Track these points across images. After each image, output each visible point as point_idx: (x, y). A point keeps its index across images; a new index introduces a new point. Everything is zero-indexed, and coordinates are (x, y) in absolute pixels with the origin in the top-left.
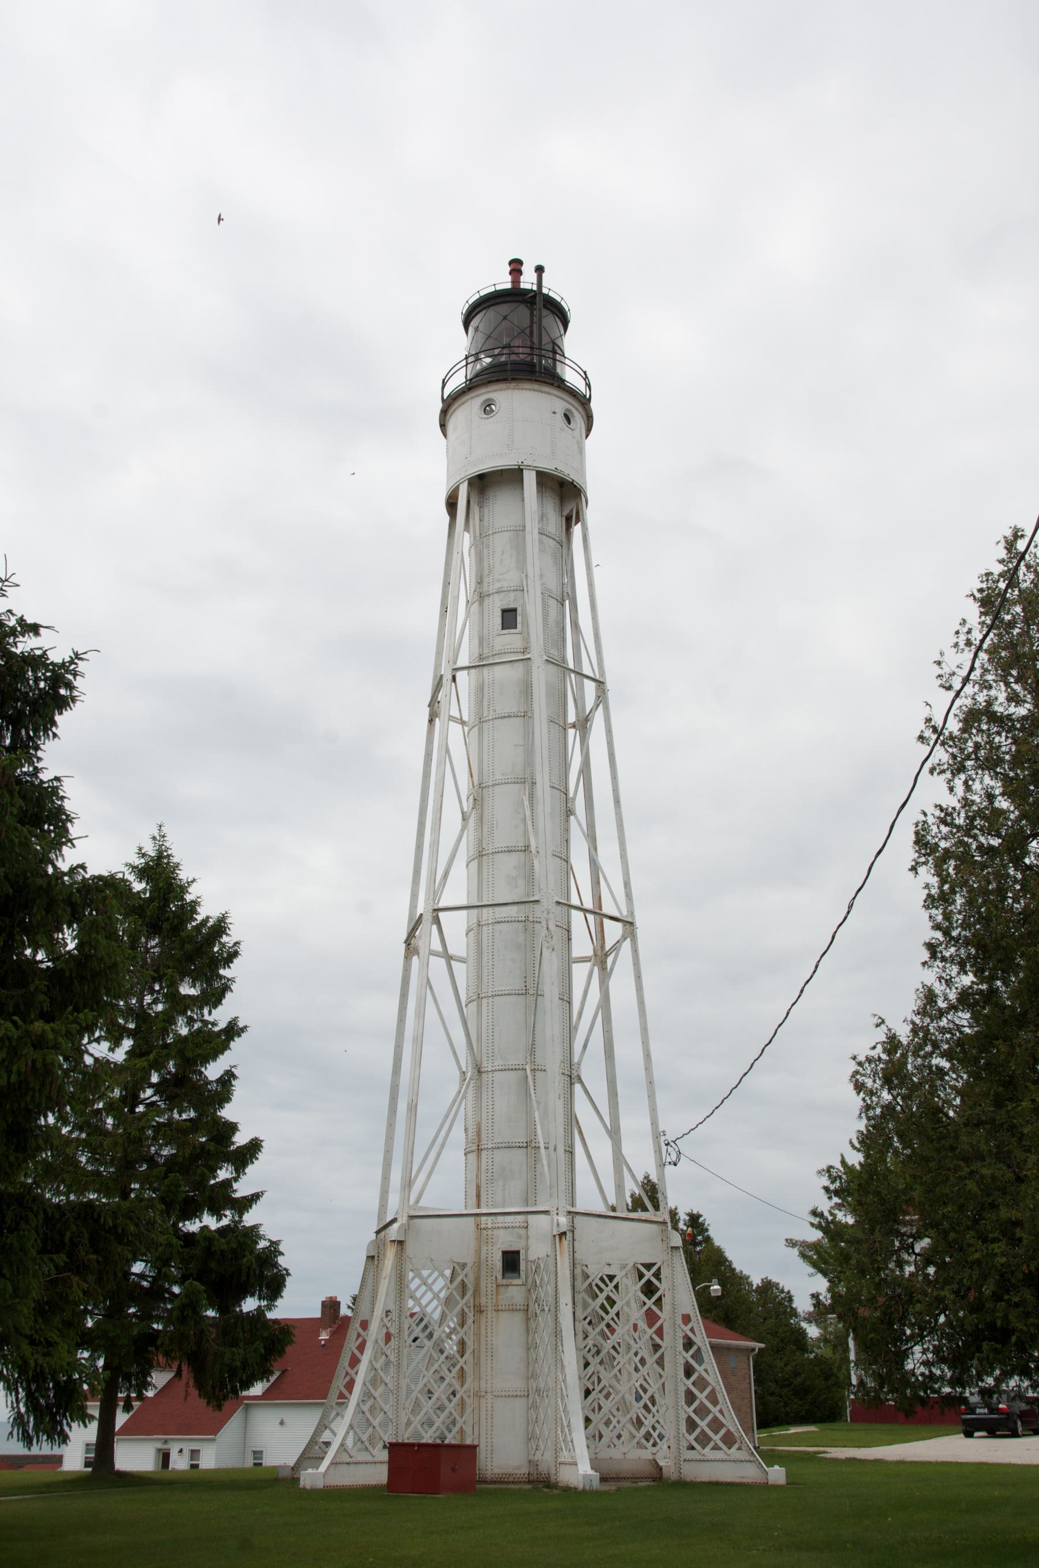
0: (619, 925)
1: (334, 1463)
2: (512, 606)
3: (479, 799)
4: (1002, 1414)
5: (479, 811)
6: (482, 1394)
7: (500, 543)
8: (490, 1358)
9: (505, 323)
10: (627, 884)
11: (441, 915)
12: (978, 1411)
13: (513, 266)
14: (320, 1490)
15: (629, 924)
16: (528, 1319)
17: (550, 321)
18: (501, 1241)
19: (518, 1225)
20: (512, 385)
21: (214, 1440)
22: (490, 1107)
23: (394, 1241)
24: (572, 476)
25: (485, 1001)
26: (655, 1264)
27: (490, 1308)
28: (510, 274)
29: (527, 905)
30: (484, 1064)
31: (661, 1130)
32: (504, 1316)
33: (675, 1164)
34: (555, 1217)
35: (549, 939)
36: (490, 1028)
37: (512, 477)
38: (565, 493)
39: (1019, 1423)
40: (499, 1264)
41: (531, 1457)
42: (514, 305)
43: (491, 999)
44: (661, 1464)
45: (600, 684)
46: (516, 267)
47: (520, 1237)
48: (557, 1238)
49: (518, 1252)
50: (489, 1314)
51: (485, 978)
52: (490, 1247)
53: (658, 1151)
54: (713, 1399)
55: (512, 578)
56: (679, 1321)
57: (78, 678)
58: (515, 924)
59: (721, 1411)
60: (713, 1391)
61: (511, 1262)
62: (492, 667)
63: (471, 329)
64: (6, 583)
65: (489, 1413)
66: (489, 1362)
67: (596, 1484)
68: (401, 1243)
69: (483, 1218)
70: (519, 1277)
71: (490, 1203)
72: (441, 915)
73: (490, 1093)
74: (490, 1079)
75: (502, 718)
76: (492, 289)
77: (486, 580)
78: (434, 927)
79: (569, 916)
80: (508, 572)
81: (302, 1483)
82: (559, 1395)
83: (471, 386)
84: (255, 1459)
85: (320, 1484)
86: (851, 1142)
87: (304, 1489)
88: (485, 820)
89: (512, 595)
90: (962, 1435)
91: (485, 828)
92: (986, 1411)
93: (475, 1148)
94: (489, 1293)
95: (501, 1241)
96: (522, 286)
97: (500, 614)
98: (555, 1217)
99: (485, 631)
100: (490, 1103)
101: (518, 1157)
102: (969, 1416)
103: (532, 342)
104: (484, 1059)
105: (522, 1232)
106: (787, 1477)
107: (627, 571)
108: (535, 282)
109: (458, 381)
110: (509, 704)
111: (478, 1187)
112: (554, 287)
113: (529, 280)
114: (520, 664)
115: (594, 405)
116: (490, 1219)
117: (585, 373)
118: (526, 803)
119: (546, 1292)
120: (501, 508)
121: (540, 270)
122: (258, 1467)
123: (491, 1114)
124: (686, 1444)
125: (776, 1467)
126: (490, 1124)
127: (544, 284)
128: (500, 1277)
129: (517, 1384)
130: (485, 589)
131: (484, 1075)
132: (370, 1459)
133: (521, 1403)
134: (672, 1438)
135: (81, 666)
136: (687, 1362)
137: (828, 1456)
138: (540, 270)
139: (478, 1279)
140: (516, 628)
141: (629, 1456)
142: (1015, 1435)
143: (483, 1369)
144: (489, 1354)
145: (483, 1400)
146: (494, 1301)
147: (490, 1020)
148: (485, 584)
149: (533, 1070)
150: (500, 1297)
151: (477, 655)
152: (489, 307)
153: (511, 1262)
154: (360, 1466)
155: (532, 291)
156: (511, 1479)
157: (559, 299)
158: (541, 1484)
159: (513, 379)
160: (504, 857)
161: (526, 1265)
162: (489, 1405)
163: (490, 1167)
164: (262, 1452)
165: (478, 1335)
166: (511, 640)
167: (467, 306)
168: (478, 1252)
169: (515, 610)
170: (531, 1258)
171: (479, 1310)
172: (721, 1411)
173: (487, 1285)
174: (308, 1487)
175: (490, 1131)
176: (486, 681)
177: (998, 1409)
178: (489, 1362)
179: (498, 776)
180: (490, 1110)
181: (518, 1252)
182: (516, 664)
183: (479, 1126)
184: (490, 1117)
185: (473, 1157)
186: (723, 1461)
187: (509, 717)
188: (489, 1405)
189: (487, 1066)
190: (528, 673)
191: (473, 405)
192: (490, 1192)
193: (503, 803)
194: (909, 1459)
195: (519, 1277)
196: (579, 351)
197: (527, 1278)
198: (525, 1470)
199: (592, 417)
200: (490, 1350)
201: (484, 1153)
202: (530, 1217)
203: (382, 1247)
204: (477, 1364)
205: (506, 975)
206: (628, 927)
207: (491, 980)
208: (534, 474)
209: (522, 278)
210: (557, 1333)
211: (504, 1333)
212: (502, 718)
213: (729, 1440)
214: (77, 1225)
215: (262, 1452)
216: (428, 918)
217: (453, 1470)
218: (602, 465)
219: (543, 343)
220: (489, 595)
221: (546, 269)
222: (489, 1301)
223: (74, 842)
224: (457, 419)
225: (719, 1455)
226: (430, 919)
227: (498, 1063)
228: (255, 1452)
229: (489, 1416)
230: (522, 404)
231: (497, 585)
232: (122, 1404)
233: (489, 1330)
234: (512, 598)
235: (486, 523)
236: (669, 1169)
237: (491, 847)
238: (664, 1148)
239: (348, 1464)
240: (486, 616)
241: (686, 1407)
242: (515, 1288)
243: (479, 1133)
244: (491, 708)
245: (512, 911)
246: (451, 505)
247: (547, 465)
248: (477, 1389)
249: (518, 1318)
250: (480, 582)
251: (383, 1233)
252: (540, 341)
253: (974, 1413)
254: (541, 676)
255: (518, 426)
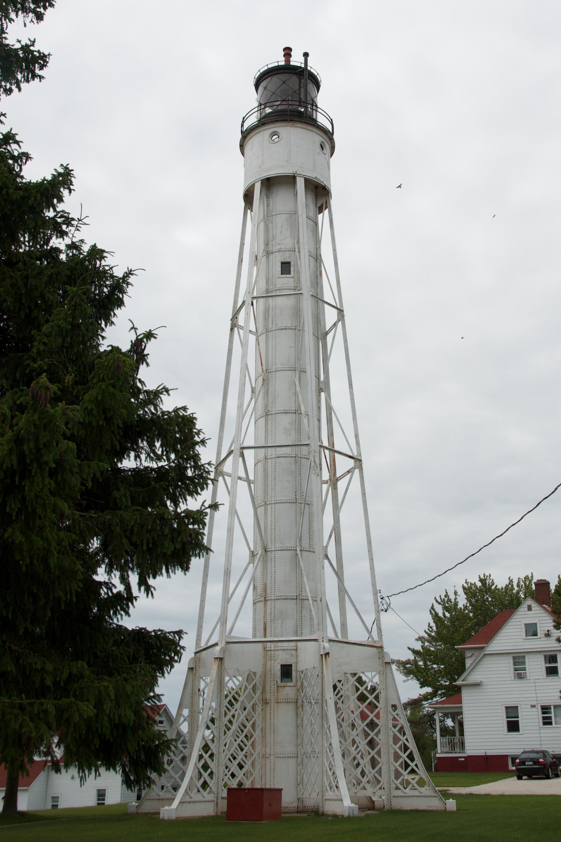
0: (352, 460)
1: (181, 803)
2: (288, 260)
3: (266, 379)
4: (541, 765)
5: (266, 387)
6: (268, 756)
7: (280, 221)
8: (272, 733)
9: (284, 85)
10: (357, 436)
11: (245, 451)
12: (527, 763)
13: (287, 51)
14: (173, 820)
15: (358, 461)
16: (297, 708)
17: (311, 87)
18: (280, 658)
19: (291, 648)
20: (290, 124)
21: (27, 790)
22: (273, 573)
23: (217, 658)
24: (325, 183)
25: (269, 507)
26: (378, 702)
27: (273, 701)
28: (284, 56)
29: (297, 447)
30: (269, 546)
31: (378, 589)
32: (282, 706)
33: (386, 611)
34: (322, 644)
35: (315, 469)
36: (273, 523)
37: (289, 180)
38: (319, 193)
39: (550, 770)
40: (279, 673)
41: (300, 796)
42: (290, 75)
43: (273, 506)
44: (374, 799)
45: (340, 311)
46: (288, 52)
47: (292, 656)
48: (324, 656)
49: (291, 665)
50: (272, 704)
51: (270, 491)
52: (273, 662)
53: (376, 602)
54: (412, 759)
55: (288, 243)
56: (390, 709)
57: (129, 286)
58: (289, 459)
59: (416, 765)
60: (411, 753)
61: (286, 671)
62: (274, 298)
63: (261, 88)
64: (80, 222)
65: (272, 768)
66: (272, 735)
67: (356, 812)
68: (221, 659)
69: (268, 644)
70: (291, 681)
71: (273, 634)
72: (245, 451)
73: (273, 564)
74: (273, 556)
75: (281, 329)
76: (276, 64)
77: (270, 243)
78: (241, 459)
79: (334, 456)
80: (285, 239)
81: (161, 816)
82: (325, 756)
83: (263, 122)
84: (53, 802)
85: (173, 817)
86: (435, 598)
87: (163, 819)
88: (270, 393)
89: (288, 254)
90: (516, 778)
91: (270, 398)
92: (531, 763)
93: (263, 599)
94: (272, 691)
95: (280, 658)
96: (292, 63)
97: (280, 265)
98: (322, 644)
99: (270, 275)
100: (273, 571)
101: (291, 605)
102: (522, 767)
103: (300, 98)
104: (269, 543)
105: (294, 652)
106: (457, 807)
107: (357, 241)
108: (303, 62)
109: (253, 120)
110: (286, 321)
111: (265, 624)
112: (314, 66)
113: (297, 60)
114: (293, 297)
115: (335, 137)
116: (273, 644)
117: (332, 120)
118: (297, 383)
119: (312, 692)
120: (281, 199)
121: (306, 55)
122: (101, 806)
123: (273, 578)
124: (394, 786)
125: (451, 800)
126: (273, 584)
127: (309, 64)
128: (279, 681)
129: (290, 749)
130: (270, 248)
131: (269, 553)
132: (202, 799)
133: (293, 762)
134: (385, 782)
135: (131, 279)
136: (395, 734)
137: (450, 792)
138: (306, 55)
139: (264, 682)
140: (290, 274)
141: (358, 795)
142: (548, 777)
143: (268, 740)
144: (272, 731)
145: (268, 761)
146: (276, 696)
147: (273, 519)
148: (270, 246)
149: (301, 550)
150: (279, 694)
151: (264, 289)
152: (274, 75)
153: (286, 671)
154: (196, 804)
155: (301, 67)
156: (286, 811)
157: (316, 74)
158: (317, 814)
159: (290, 120)
160: (282, 416)
161: (297, 674)
162: (272, 763)
163: (273, 611)
164: (58, 797)
165: (264, 718)
166: (287, 281)
167: (259, 74)
168: (265, 665)
169: (289, 263)
170: (300, 669)
171: (265, 702)
172: (416, 765)
173: (271, 686)
174: (166, 818)
175: (273, 589)
176: (271, 306)
177: (539, 762)
178: (272, 735)
179: (279, 366)
180: (273, 575)
181: (291, 665)
182: (290, 297)
183: (265, 586)
184: (273, 580)
185: (260, 605)
186: (417, 796)
187: (286, 329)
188: (272, 763)
189: (270, 547)
190: (298, 302)
191: (264, 134)
192: (273, 627)
193: (281, 382)
194: (507, 793)
195: (291, 681)
196: (328, 102)
197: (297, 681)
198: (295, 805)
199: (334, 147)
200: (272, 728)
201: (269, 602)
202: (299, 644)
203: (198, 662)
204: (264, 737)
205: (283, 490)
206: (358, 462)
207: (273, 493)
208: (303, 180)
209: (291, 59)
210: (324, 716)
211: (282, 717)
212: (281, 329)
213: (421, 783)
214: (134, 645)
215: (58, 797)
216: (237, 452)
217: (270, 805)
218: (340, 176)
219: (308, 99)
220: (273, 253)
221: (310, 55)
222: (272, 696)
223: (170, 392)
224: (254, 142)
225: (415, 793)
226: (239, 454)
227: (278, 546)
228: (53, 798)
229: (272, 771)
230: (293, 135)
231: (278, 247)
232: (62, 764)
233: (272, 716)
234: (288, 256)
235: (271, 208)
236: (382, 613)
237: (274, 410)
238: (380, 600)
239: (190, 802)
240: (271, 265)
241: (394, 763)
242: (289, 688)
243: (265, 590)
244: (274, 323)
245: (287, 450)
246: (248, 197)
247: (311, 175)
248: (264, 753)
249: (292, 707)
250: (267, 245)
251: (199, 654)
252: (306, 98)
253: (525, 765)
254: (307, 304)
255: (288, 149)
